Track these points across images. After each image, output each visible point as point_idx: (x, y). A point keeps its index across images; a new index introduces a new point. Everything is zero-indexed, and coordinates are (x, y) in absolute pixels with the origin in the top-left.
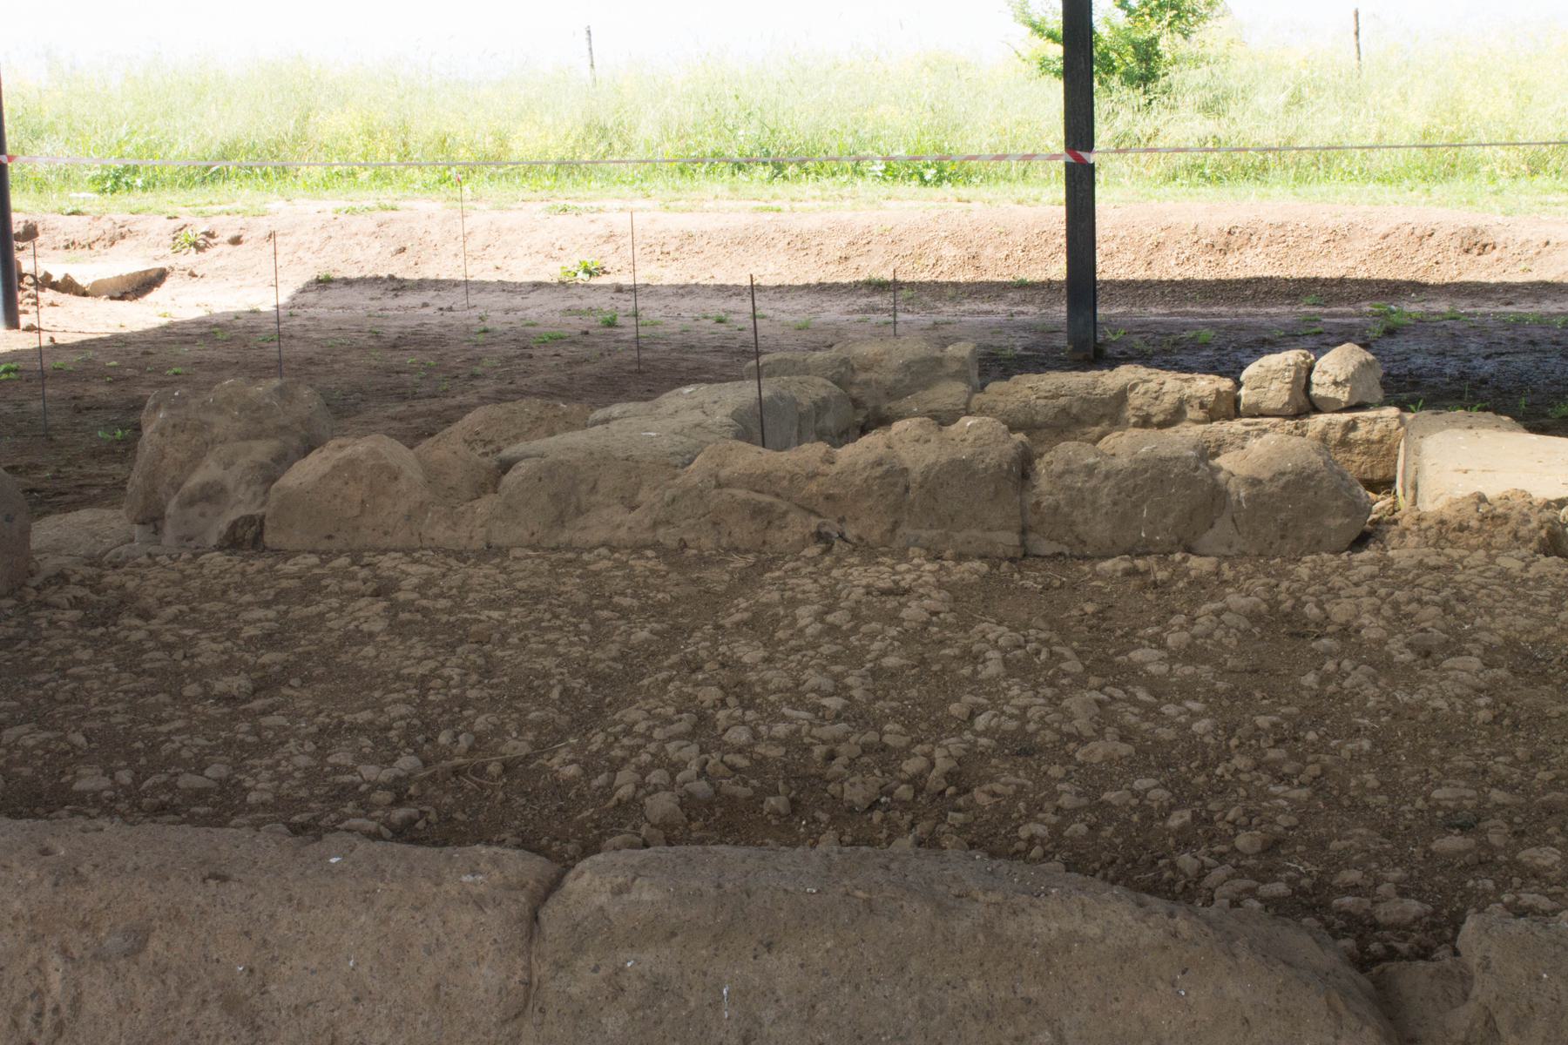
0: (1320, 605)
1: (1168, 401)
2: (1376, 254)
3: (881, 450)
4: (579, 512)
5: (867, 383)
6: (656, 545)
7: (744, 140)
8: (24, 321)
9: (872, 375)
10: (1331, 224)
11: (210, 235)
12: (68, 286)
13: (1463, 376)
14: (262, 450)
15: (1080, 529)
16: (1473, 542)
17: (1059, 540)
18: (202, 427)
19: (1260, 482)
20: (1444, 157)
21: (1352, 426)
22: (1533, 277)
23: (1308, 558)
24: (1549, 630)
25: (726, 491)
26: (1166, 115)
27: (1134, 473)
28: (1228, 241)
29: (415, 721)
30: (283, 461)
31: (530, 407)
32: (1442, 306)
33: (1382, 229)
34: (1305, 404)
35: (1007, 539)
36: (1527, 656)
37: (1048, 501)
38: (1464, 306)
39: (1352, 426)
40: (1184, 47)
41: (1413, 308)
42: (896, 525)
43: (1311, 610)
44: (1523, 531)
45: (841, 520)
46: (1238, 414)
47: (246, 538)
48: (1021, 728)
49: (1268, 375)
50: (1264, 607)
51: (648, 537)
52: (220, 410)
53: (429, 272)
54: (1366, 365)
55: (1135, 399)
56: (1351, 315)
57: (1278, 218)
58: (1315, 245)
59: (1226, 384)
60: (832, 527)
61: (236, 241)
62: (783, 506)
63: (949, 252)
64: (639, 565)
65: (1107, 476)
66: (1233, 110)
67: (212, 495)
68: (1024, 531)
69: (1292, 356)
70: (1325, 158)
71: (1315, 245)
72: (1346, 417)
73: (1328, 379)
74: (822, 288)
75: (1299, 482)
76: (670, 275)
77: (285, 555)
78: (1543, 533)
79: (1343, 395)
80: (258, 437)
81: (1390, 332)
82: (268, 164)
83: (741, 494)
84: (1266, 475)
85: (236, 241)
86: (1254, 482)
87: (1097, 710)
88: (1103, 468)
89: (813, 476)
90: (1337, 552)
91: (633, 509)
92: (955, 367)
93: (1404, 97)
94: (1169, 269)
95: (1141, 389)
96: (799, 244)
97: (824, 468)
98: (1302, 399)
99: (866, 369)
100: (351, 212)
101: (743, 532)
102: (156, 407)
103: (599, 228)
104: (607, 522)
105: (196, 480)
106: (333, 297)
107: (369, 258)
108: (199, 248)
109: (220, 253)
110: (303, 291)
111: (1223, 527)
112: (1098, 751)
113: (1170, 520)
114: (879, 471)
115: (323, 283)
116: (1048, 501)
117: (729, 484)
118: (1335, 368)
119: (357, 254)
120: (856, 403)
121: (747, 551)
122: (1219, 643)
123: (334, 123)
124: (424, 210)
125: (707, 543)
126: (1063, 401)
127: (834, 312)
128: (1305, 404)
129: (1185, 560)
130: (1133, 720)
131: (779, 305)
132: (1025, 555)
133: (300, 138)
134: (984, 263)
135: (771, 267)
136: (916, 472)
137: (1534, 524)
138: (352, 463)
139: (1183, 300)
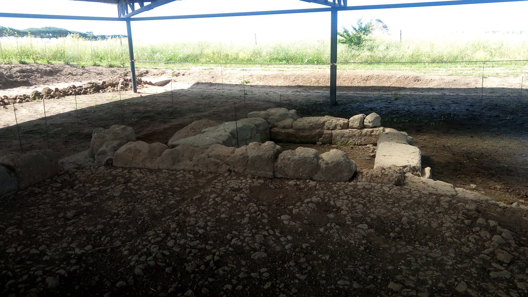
0: (334, 202)
1: (333, 125)
2: (397, 81)
3: (244, 151)
4: (179, 161)
5: (272, 119)
6: (194, 171)
7: (281, 56)
8: (138, 91)
9: (273, 117)
10: (388, 75)
11: (179, 73)
12: (150, 84)
13: (408, 111)
14: (115, 143)
15: (286, 172)
16: (379, 181)
17: (282, 174)
18: (104, 137)
19: (328, 164)
20: (414, 61)
21: (372, 131)
22: (428, 87)
23: (338, 183)
24: (389, 214)
25: (210, 158)
26: (362, 51)
27: (299, 160)
28: (368, 78)
29: (100, 231)
30: (120, 145)
31: (204, 121)
32: (409, 93)
33: (398, 76)
34: (362, 126)
35: (270, 174)
36: (382, 222)
37: (279, 165)
38: (413, 93)
39: (372, 131)
40: (367, 38)
41: (402, 93)
42: (245, 169)
43: (332, 203)
44: (391, 179)
45: (234, 167)
46: (348, 128)
47: (109, 164)
48: (242, 244)
49: (355, 119)
50: (321, 201)
51: (192, 168)
52: (108, 134)
53: (217, 82)
54: (377, 118)
55: (326, 124)
56: (389, 95)
57: (378, 74)
58: (385, 80)
59: (346, 121)
60: (232, 168)
61: (183, 75)
62: (221, 163)
63: (313, 80)
64: (188, 176)
65: (292, 161)
66: (375, 50)
67: (104, 153)
68: (274, 172)
69: (360, 116)
70: (391, 61)
71: (385, 80)
72: (371, 129)
73: (367, 121)
74: (289, 87)
75: (338, 164)
76: (261, 83)
77: (116, 168)
78: (396, 179)
79: (371, 125)
80: (116, 140)
81: (396, 99)
82: (194, 59)
83: (213, 159)
84: (330, 162)
85: (183, 75)
86: (327, 164)
87: (263, 239)
88: (292, 159)
89: (228, 156)
90: (345, 181)
91: (191, 161)
92: (290, 115)
93: (408, 48)
94: (356, 84)
95: (328, 122)
96: (286, 78)
97: (231, 155)
98: (362, 125)
99: (272, 115)
100: (205, 69)
101: (213, 169)
102: (95, 132)
103: (249, 74)
104: (186, 164)
105: (100, 150)
106: (199, 86)
107: (207, 79)
108: (177, 76)
109: (180, 77)
110: (194, 85)
111: (319, 174)
112: (256, 256)
113: (307, 172)
114: (242, 157)
115: (198, 83)
116: (279, 165)
117: (211, 157)
118: (370, 118)
119: (205, 78)
120: (269, 123)
121: (213, 173)
122: (306, 213)
123: (208, 51)
124: (218, 69)
125: (205, 171)
126: (311, 124)
127: (290, 92)
128: (362, 126)
129: (309, 182)
130: (271, 242)
131: (280, 90)
132: (274, 177)
133: (201, 54)
134: (320, 82)
135: (280, 82)
136: (250, 157)
137: (394, 177)
138: (130, 149)
139: (357, 90)
